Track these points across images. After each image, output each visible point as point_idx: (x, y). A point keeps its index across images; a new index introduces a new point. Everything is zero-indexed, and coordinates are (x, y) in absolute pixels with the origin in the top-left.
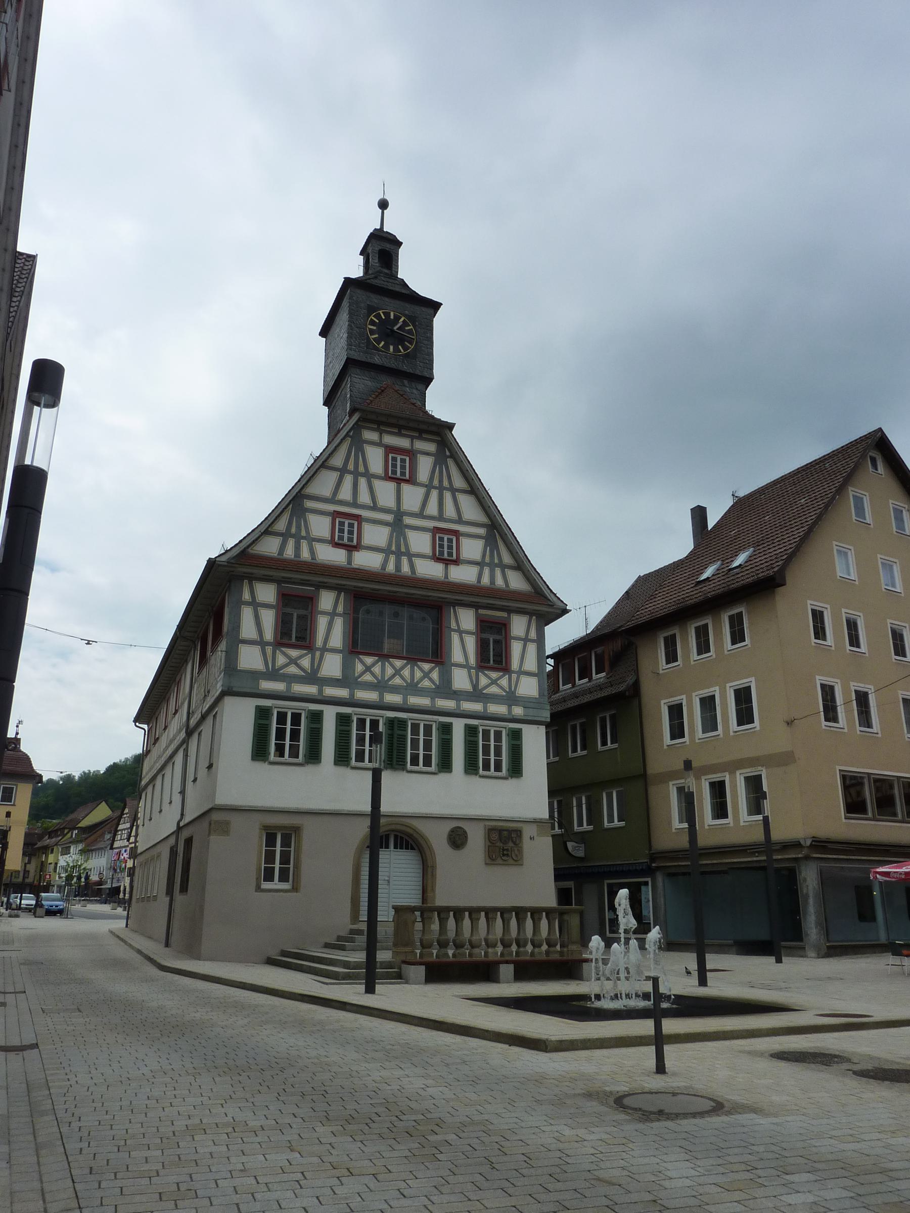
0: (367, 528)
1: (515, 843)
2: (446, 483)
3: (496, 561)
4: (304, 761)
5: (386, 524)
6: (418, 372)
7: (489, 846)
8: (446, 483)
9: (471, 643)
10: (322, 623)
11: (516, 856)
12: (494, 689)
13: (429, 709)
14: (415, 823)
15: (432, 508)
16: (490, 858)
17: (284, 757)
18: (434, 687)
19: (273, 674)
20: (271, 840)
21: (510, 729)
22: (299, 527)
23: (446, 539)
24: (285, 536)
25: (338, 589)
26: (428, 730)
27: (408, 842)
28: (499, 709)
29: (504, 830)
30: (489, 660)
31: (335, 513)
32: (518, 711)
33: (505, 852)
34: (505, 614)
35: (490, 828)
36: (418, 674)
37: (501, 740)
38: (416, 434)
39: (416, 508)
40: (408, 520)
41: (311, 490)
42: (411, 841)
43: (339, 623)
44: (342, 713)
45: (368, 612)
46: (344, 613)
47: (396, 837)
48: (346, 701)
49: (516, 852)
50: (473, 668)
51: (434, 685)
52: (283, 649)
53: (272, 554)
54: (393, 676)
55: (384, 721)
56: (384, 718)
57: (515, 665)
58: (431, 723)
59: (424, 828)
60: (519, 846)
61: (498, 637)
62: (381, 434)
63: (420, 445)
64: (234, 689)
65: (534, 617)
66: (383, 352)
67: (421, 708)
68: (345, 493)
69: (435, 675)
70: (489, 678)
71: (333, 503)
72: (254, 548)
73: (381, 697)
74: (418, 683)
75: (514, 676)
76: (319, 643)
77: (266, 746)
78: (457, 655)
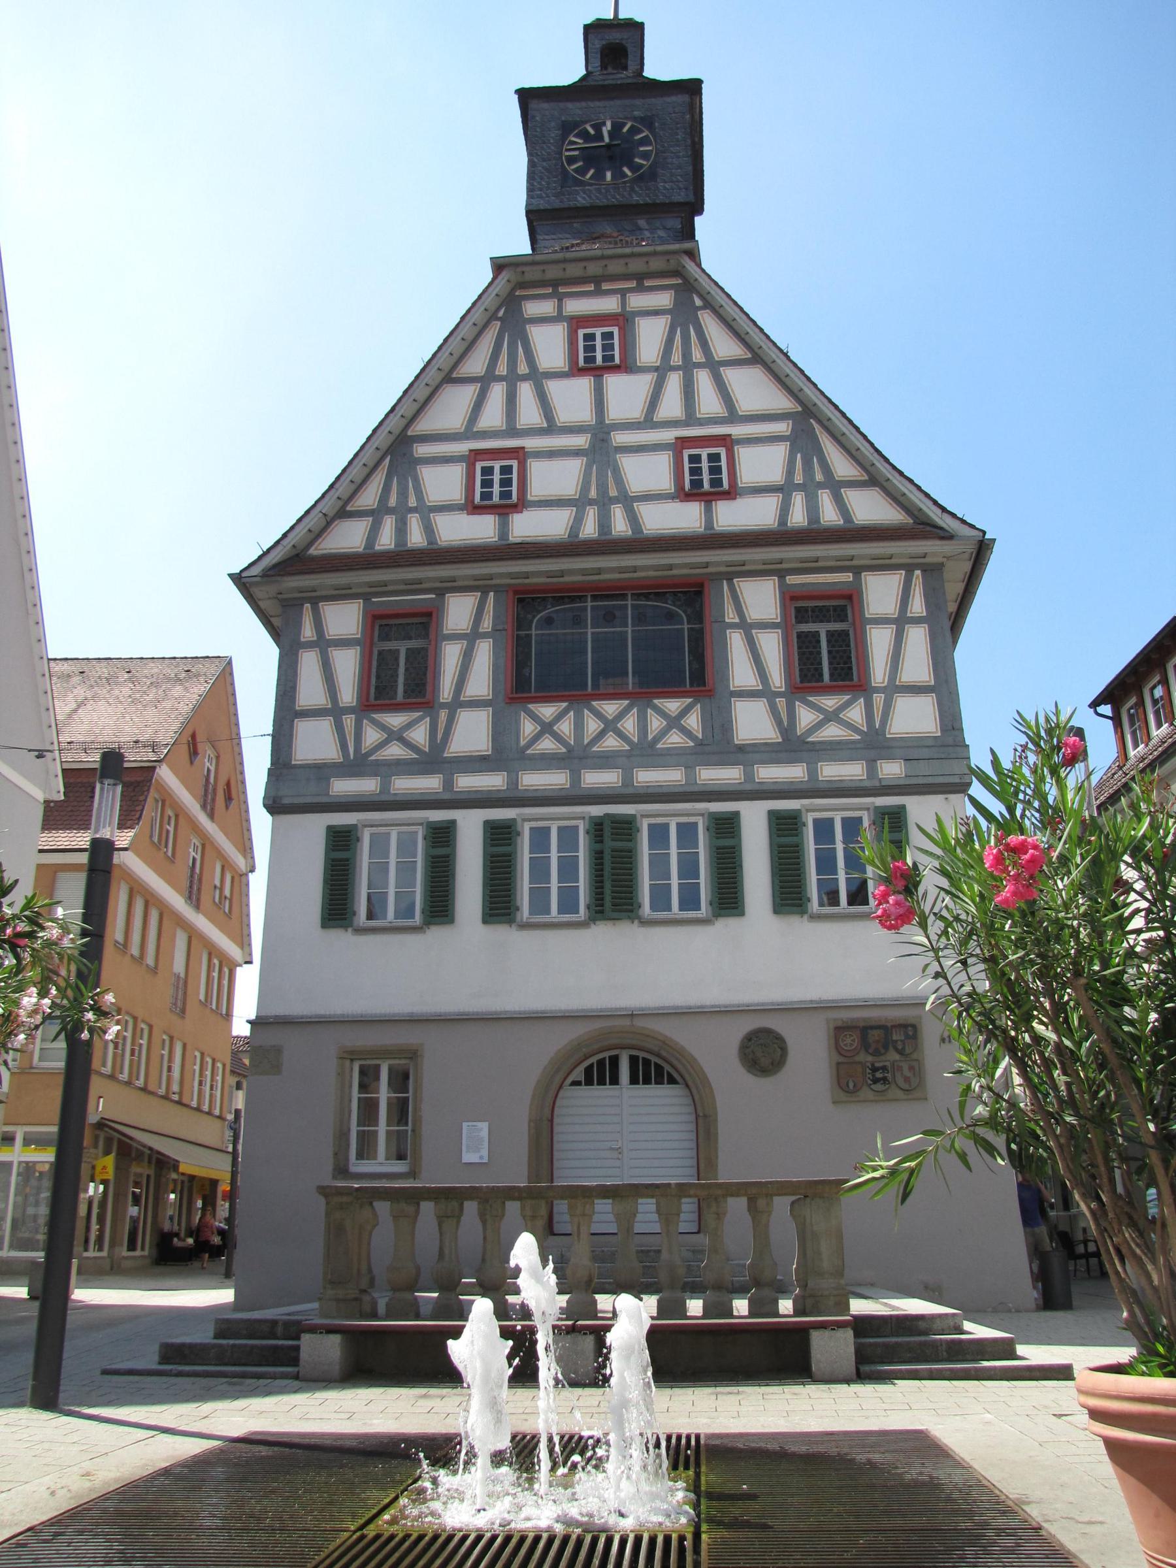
0: (536, 469)
1: (901, 1052)
2: (697, 355)
3: (819, 477)
4: (710, 912)
5: (576, 453)
6: (661, 199)
7: (838, 1064)
8: (697, 355)
9: (771, 645)
10: (451, 655)
11: (907, 1079)
12: (832, 732)
13: (681, 790)
14: (664, 1028)
15: (671, 405)
16: (841, 1087)
17: (839, 905)
18: (692, 744)
19: (357, 765)
20: (368, 1078)
21: (711, 814)
22: (403, 494)
23: (704, 458)
24: (376, 515)
25: (481, 587)
26: (687, 832)
27: (662, 1068)
28: (852, 771)
29: (872, 1028)
30: (821, 675)
31: (679, 441)
32: (891, 770)
33: (879, 1075)
34: (848, 577)
35: (840, 1024)
36: (656, 723)
37: (388, 852)
38: (633, 284)
39: (636, 412)
40: (620, 438)
41: (426, 424)
42: (667, 1068)
43: (484, 652)
44: (493, 821)
45: (549, 621)
46: (495, 630)
47: (633, 1060)
48: (804, 786)
49: (907, 1073)
50: (780, 695)
51: (692, 740)
52: (810, 699)
53: (386, 547)
54: (601, 735)
55: (587, 827)
56: (587, 818)
57: (879, 673)
58: (692, 819)
59: (683, 1036)
60: (915, 1056)
61: (414, 644)
62: (560, 300)
63: (637, 301)
64: (286, 801)
65: (918, 572)
66: (591, 185)
67: (665, 790)
68: (493, 416)
69: (693, 721)
70: (819, 709)
71: (468, 439)
72: (321, 546)
73: (872, 770)
74: (656, 740)
75: (878, 699)
76: (446, 692)
77: (331, 895)
78: (742, 674)
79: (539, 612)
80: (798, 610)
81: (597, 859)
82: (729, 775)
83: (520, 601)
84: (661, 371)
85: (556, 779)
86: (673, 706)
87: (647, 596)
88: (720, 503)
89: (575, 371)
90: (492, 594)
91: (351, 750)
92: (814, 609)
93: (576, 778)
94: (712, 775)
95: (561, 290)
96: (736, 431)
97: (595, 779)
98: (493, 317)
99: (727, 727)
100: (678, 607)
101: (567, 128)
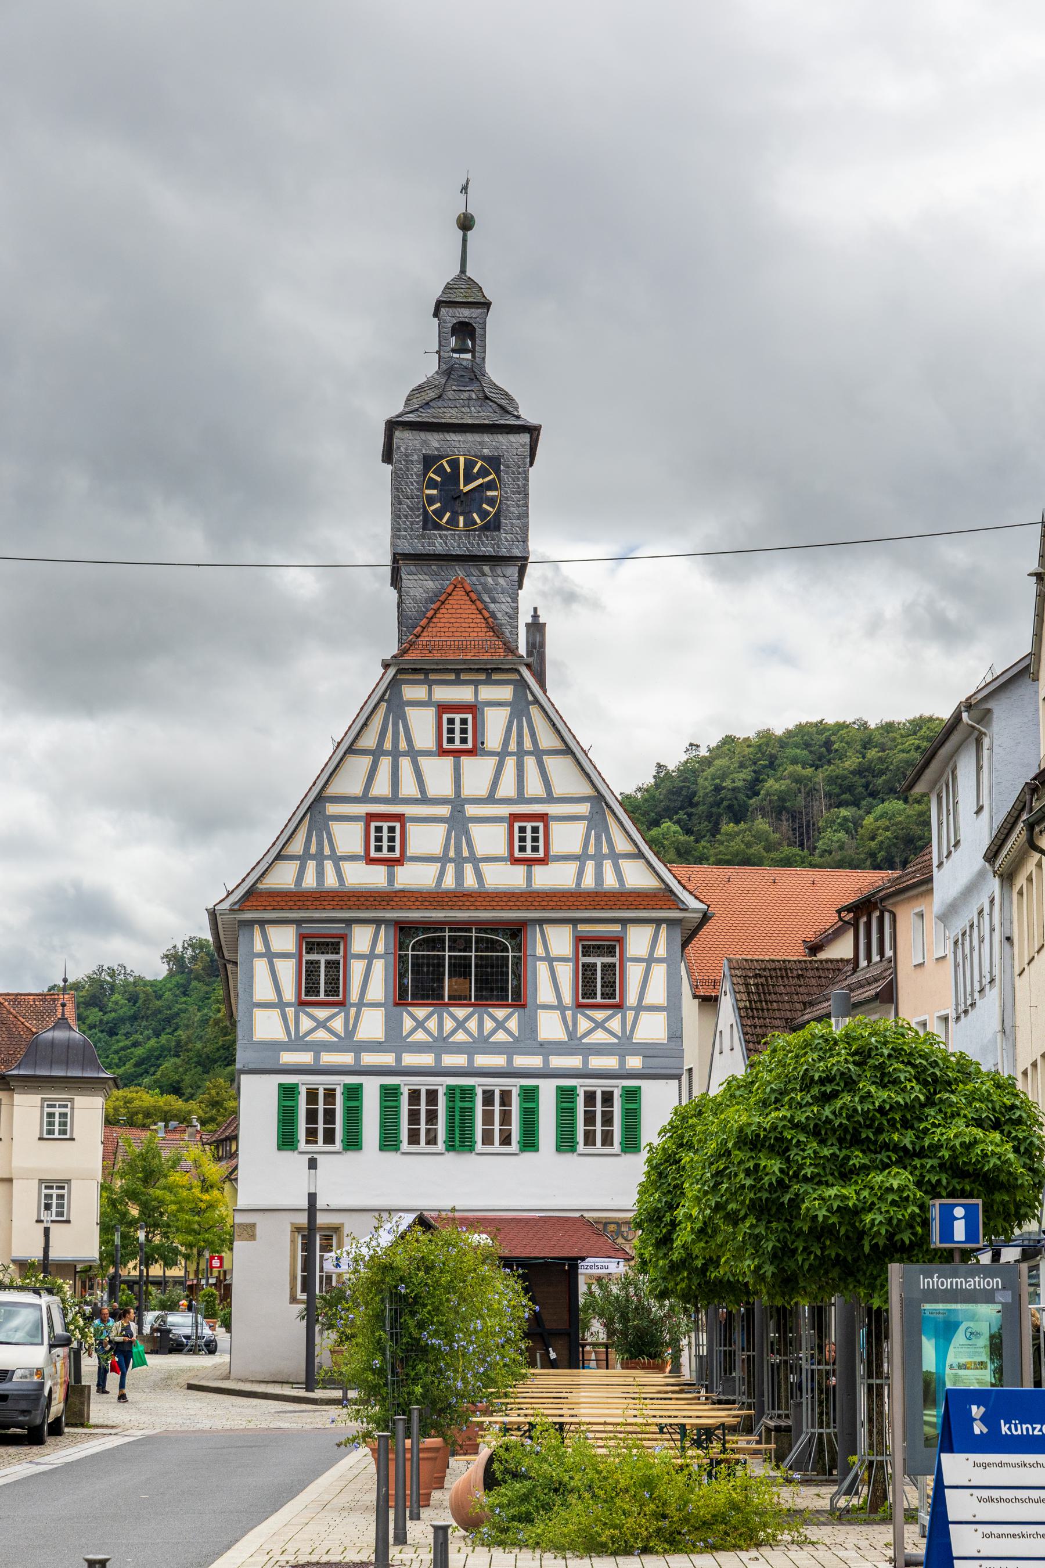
3: (605, 850)
8: (528, 745)
9: (565, 972)
15: (507, 788)
19: (297, 1043)
28: (610, 1063)
32: (634, 1062)
34: (617, 928)
38: (483, 677)
39: (483, 792)
40: (471, 810)
41: (335, 789)
43: (379, 967)
62: (430, 687)
63: (487, 693)
66: (448, 529)
68: (382, 787)
69: (513, 1024)
78: (545, 993)
79: (414, 938)
80: (584, 947)
81: (451, 1111)
82: (534, 1062)
83: (401, 929)
84: (502, 755)
85: (427, 1060)
86: (500, 1013)
87: (485, 931)
88: (537, 867)
89: (443, 752)
90: (383, 926)
91: (293, 1033)
92: (594, 947)
93: (438, 1059)
94: (521, 1061)
95: (432, 677)
96: (552, 809)
97: (451, 1060)
98: (382, 699)
99: (534, 1030)
100: (506, 939)
101: (429, 461)
